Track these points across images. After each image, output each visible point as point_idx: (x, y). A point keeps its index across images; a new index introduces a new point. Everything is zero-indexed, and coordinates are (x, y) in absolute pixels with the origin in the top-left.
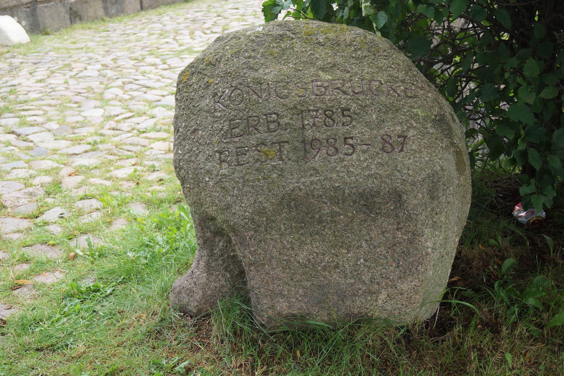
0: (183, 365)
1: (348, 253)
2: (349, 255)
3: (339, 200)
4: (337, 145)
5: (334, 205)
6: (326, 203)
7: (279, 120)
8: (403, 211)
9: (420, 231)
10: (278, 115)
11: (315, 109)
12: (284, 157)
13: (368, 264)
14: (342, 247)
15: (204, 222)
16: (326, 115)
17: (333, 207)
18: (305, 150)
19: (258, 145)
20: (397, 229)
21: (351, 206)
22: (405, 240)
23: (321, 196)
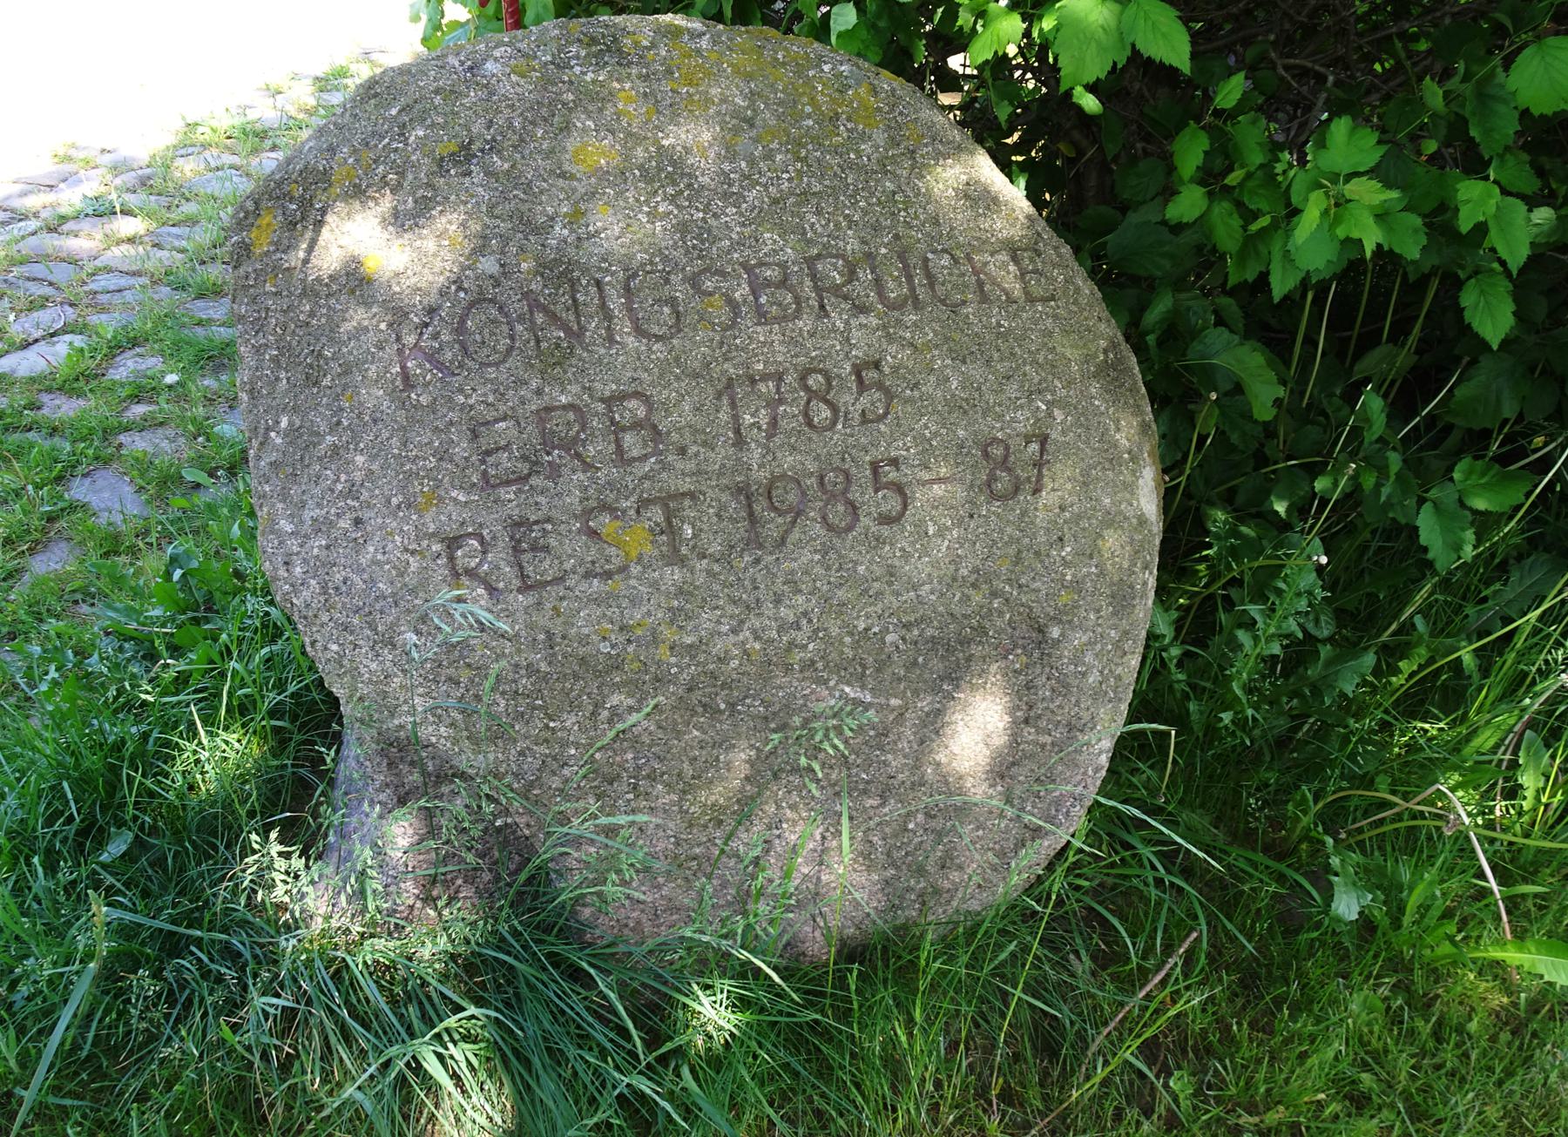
0: (794, 996)
1: (883, 805)
2: (886, 810)
3: (864, 667)
4: (855, 495)
5: (848, 684)
6: (826, 682)
7: (655, 419)
8: (1047, 670)
9: (1086, 716)
10: (647, 400)
11: (772, 369)
12: (684, 550)
13: (933, 824)
14: (865, 792)
15: (1118, 28)
16: (807, 388)
17: (847, 689)
18: (751, 514)
19: (588, 513)
20: (1026, 721)
21: (899, 679)
22: (1043, 746)
23: (813, 662)
